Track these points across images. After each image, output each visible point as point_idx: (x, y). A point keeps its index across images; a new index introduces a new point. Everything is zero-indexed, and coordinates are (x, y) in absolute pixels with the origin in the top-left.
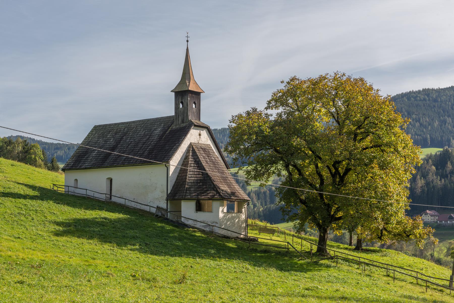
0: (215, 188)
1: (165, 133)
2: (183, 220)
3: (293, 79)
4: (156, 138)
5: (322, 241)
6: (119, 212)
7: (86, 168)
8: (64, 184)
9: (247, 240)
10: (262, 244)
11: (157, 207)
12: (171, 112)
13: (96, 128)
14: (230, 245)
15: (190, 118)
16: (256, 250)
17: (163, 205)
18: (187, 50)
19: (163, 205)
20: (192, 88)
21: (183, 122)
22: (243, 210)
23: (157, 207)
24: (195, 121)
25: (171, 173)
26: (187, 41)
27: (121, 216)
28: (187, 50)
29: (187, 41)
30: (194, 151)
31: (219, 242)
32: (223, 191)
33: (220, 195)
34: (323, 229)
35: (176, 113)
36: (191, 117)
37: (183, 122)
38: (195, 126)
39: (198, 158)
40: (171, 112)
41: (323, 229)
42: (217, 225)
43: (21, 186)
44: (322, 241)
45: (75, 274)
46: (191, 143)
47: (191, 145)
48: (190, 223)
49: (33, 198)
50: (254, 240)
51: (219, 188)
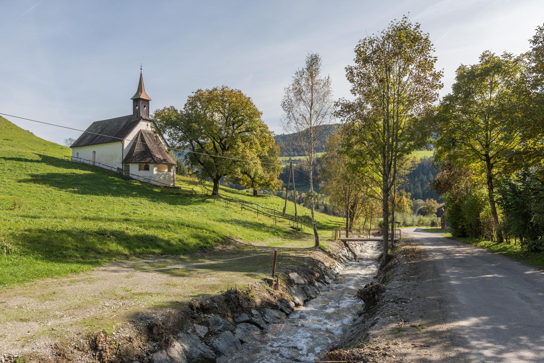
0: (152, 156)
1: (127, 124)
2: (130, 175)
3: (199, 91)
4: (121, 127)
5: (216, 188)
6: (88, 170)
7: (82, 146)
8: (345, 219)
9: (174, 188)
10: (183, 191)
11: (118, 168)
12: (131, 113)
13: (94, 123)
14: (157, 190)
15: (141, 115)
16: (173, 193)
17: (120, 166)
18: (141, 74)
19: (121, 167)
20: (143, 96)
21: (137, 118)
22: (172, 170)
23: (118, 168)
24: (144, 117)
25: (125, 147)
26: (141, 69)
27: (89, 172)
28: (141, 74)
29: (141, 69)
30: (142, 135)
31: (496, 275)
32: (157, 158)
33: (154, 160)
34: (216, 181)
35: (134, 112)
36: (142, 114)
37: (137, 118)
38: (143, 119)
39: (144, 138)
40: (131, 113)
41: (216, 181)
42: (152, 179)
43: (37, 155)
44: (216, 188)
45: (229, 267)
46: (140, 130)
47: (140, 131)
48: (135, 177)
49: (38, 161)
50: (179, 188)
51: (155, 156)
